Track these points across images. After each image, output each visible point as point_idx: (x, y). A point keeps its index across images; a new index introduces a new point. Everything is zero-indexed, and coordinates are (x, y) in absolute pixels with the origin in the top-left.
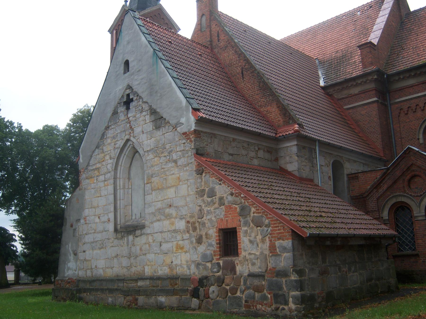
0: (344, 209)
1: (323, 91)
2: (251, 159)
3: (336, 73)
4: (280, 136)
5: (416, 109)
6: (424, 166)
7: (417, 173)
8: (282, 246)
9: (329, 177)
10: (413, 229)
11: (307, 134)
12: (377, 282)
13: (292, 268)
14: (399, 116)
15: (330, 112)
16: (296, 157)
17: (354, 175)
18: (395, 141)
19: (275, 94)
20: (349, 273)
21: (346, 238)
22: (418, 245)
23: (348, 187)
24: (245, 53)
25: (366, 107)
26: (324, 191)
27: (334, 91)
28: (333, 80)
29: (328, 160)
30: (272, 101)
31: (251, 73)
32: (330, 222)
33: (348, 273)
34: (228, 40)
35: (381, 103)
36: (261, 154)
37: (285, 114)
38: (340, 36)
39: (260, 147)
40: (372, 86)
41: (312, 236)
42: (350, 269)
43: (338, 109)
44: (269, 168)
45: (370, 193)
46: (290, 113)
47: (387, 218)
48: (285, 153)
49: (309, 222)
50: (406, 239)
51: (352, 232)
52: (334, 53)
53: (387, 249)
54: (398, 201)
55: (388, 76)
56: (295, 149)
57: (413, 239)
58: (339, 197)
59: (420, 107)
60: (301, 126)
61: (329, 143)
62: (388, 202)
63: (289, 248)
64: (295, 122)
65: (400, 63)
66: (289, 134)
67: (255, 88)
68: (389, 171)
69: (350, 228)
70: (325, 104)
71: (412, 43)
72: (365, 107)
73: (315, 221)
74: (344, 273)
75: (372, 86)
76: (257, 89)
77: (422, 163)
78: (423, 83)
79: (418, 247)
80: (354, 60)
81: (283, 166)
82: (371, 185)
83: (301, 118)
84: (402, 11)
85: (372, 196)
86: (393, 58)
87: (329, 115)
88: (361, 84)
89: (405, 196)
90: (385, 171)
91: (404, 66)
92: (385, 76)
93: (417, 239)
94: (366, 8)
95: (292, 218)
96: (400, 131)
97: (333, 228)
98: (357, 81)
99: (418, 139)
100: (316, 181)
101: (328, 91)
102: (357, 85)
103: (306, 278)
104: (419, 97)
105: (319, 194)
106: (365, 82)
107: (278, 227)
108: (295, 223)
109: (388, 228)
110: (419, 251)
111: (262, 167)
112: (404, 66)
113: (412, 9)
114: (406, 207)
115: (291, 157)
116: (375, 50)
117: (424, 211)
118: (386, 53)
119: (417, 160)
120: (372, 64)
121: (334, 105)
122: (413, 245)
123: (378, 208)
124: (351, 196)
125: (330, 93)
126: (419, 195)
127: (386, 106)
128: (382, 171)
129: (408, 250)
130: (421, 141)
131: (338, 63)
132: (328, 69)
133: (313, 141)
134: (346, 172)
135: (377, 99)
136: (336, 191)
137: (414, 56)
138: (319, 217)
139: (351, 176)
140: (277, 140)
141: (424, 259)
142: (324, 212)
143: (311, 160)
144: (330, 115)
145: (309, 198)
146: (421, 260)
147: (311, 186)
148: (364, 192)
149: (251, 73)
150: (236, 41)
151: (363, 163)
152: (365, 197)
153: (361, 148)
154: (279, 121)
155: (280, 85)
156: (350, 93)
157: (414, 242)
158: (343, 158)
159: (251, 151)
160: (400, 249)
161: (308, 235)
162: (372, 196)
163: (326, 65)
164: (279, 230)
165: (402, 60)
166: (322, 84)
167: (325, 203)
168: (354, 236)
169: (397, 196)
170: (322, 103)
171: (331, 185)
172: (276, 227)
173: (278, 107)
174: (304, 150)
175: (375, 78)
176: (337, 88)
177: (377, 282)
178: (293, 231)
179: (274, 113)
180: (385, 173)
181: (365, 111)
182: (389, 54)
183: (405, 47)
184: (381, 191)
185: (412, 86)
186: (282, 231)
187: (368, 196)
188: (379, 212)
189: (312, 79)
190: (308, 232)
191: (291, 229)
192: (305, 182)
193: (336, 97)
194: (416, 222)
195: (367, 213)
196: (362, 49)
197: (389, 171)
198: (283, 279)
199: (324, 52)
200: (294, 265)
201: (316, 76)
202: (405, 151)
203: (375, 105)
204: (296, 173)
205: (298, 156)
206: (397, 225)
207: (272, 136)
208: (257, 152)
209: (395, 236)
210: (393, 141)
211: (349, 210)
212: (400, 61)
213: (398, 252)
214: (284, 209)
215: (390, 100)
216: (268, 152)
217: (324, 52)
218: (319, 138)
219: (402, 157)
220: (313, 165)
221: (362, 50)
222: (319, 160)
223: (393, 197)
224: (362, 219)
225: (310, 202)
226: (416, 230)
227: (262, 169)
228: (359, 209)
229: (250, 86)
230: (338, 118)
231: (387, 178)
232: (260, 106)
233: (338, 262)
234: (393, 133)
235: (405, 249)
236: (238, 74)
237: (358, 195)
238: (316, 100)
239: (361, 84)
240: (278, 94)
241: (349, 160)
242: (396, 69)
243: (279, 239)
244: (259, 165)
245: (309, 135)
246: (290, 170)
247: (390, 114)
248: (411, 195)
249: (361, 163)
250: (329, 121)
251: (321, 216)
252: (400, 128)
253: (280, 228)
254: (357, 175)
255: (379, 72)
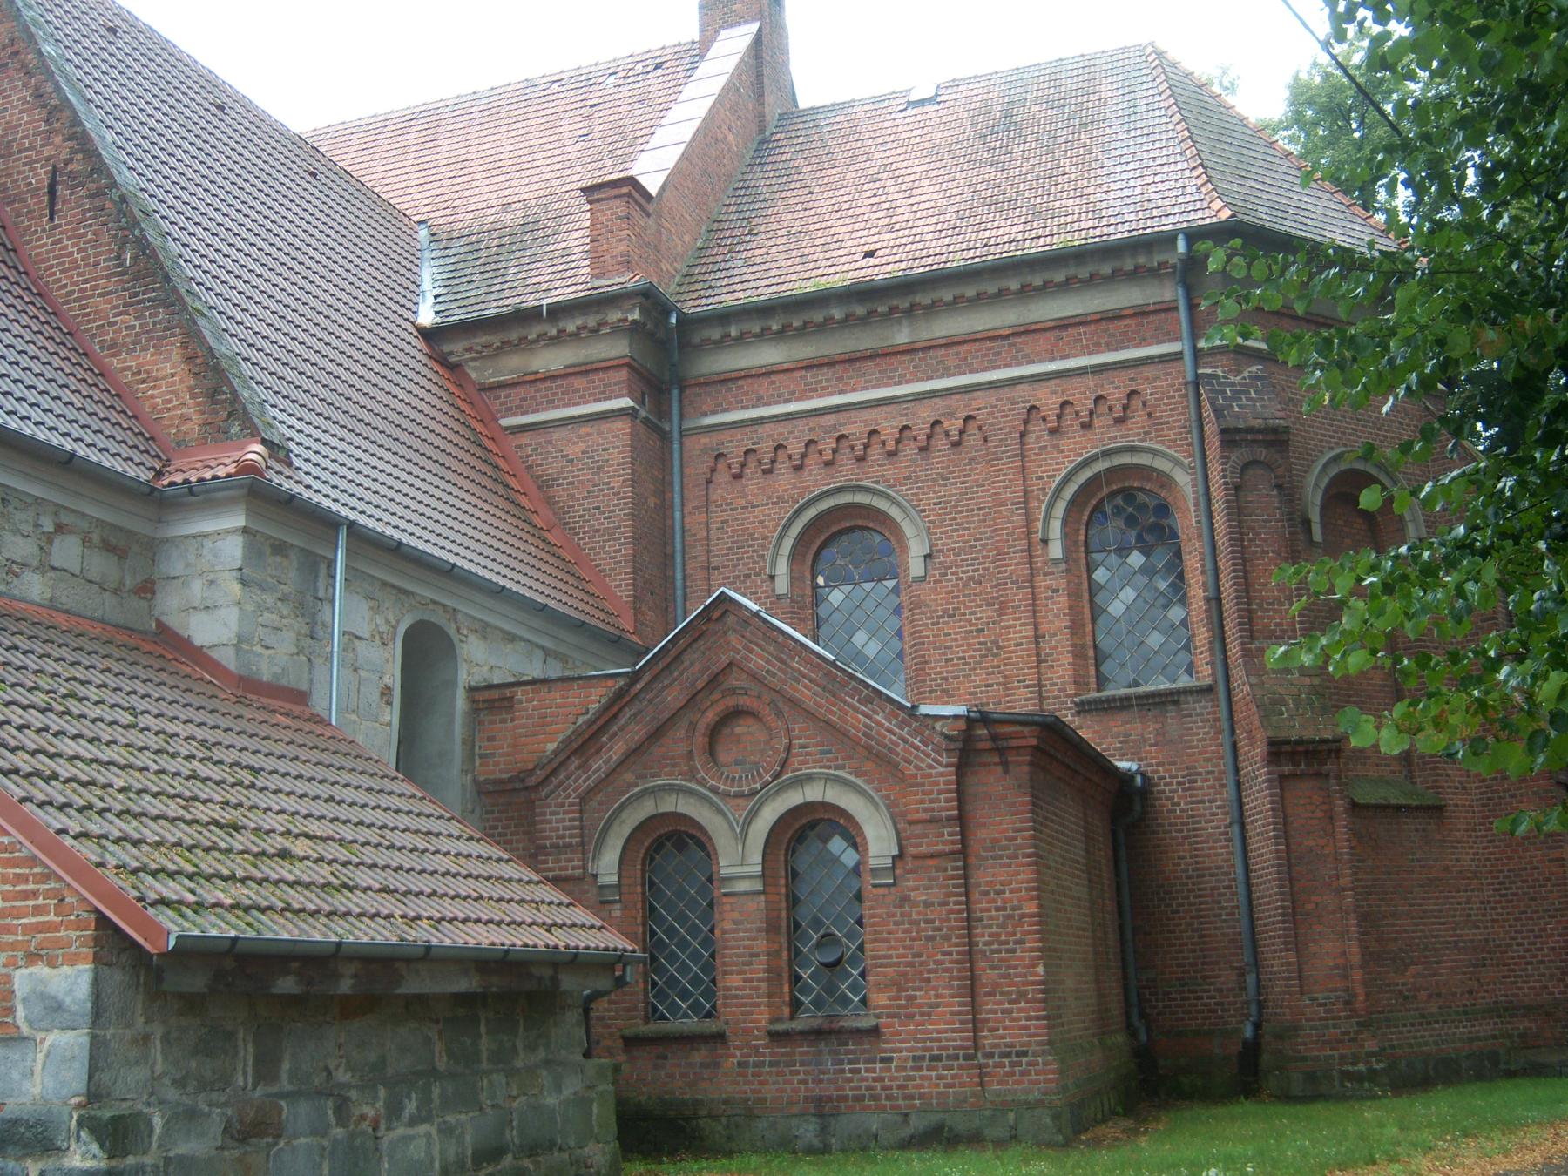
0: (416, 832)
1: (421, 344)
2: (9, 571)
3: (489, 282)
4: (172, 484)
5: (773, 461)
6: (774, 675)
7: (744, 701)
8: (43, 997)
9: (386, 692)
10: (712, 931)
11: (297, 489)
12: (527, 1163)
13: (79, 1106)
14: (709, 482)
15: (438, 429)
16: (236, 588)
17: (496, 694)
18: (684, 578)
19: (180, 299)
20: (388, 1129)
21: (382, 964)
22: (726, 998)
23: (469, 743)
24: (80, 108)
25: (586, 429)
26: (343, 747)
27: (470, 350)
28: (470, 309)
29: (391, 618)
30: (166, 329)
31: (92, 196)
32: (323, 887)
33: (383, 1126)
34: (12, 40)
35: (646, 421)
36: (67, 552)
37: (212, 394)
38: (526, 151)
39: (65, 519)
40: (619, 348)
41: (191, 952)
42: (394, 1110)
43: (474, 424)
44: (102, 621)
45: (554, 772)
46: (234, 393)
47: (614, 879)
48: (188, 565)
49: (208, 878)
50: (684, 968)
51: (422, 934)
52: (493, 211)
53: (587, 1011)
54: (661, 810)
55: (684, 320)
56: (233, 550)
57: (708, 968)
58: (421, 785)
59: (790, 457)
60: (282, 454)
61: (400, 543)
62: (624, 815)
63: (74, 1008)
64: (251, 431)
65: (737, 279)
66: (215, 477)
67: (97, 264)
68: (638, 686)
69: (418, 917)
70: (422, 393)
71: (790, 216)
72: (584, 430)
73: (240, 873)
74: (365, 1125)
75: (619, 348)
76: (108, 268)
77: (768, 662)
78: (809, 367)
79: (725, 1005)
80: (564, 245)
81: (173, 621)
82: (560, 737)
83: (285, 423)
84: (769, 99)
85: (561, 783)
86: (711, 259)
87: (431, 438)
88: (575, 336)
89: (691, 792)
90: (621, 682)
91: (748, 293)
92: (674, 320)
93: (725, 973)
94: (640, 66)
95: (117, 855)
96: (708, 538)
97: (329, 915)
98: (561, 325)
99: (772, 577)
100: (318, 704)
101: (446, 348)
102: (560, 339)
103: (148, 1160)
104: (789, 417)
105: (316, 756)
106: (595, 331)
107: (34, 894)
108: (122, 882)
109: (598, 923)
110: (727, 1023)
111: (67, 612)
112: (748, 293)
113: (804, 103)
114: (692, 837)
115: (212, 582)
116: (648, 215)
117: (756, 857)
118: (687, 238)
119: (751, 651)
120: (627, 264)
121: (463, 406)
122: (710, 994)
123: (582, 836)
124: (475, 781)
125: (453, 359)
126: (746, 790)
127: (665, 437)
128: (610, 683)
129: (686, 1015)
130: (782, 586)
131: (503, 250)
132: (461, 265)
133: (326, 523)
134: (465, 676)
135: (632, 404)
136: (412, 757)
137: (789, 262)
138: (271, 857)
139: (486, 695)
140: (161, 501)
141: (743, 1055)
142: (307, 836)
143: (308, 608)
144: (437, 441)
145: (256, 771)
146: (734, 1056)
147: (285, 721)
148: (530, 766)
149: (92, 196)
150: (48, 49)
151: (543, 648)
152: (536, 788)
153: (542, 588)
154: (185, 419)
155: (299, 349)
156: (534, 369)
157: (714, 981)
158: (460, 616)
159: (16, 532)
160: (655, 1009)
161: (172, 944)
162: (561, 783)
163: (454, 251)
164: (38, 910)
165: (744, 270)
166: (426, 317)
167: (331, 799)
168: (428, 956)
169: (662, 788)
170: (410, 386)
171: (389, 724)
172: (26, 895)
173: (189, 359)
174: (278, 559)
175: (634, 321)
176: (480, 340)
177: (527, 1163)
178: (102, 921)
179: (166, 380)
180: (620, 694)
181: (582, 446)
182: (699, 243)
183: (762, 228)
184: (599, 766)
185: (768, 373)
186: (52, 917)
187: (545, 781)
188: (584, 853)
189: (385, 290)
190: (173, 928)
191: (97, 911)
192: (265, 701)
193: (473, 375)
194: (725, 900)
195: (533, 856)
196: (598, 201)
197: (638, 686)
198: (29, 1163)
199: (456, 203)
200: (94, 1095)
201: (407, 283)
202: (706, 607)
203: (623, 426)
204: (227, 658)
205: (243, 582)
206: (652, 909)
207: (135, 480)
208: (50, 542)
209: (621, 959)
210: (679, 576)
211: (438, 835)
212: (736, 272)
213: (647, 1020)
214: (90, 807)
215: (682, 417)
216: (108, 547)
217: (456, 203)
218: (353, 516)
219: (695, 633)
220: (315, 631)
221: (596, 205)
222: (345, 610)
223: (644, 793)
224: (488, 878)
225: (253, 786)
226: (724, 932)
227: (60, 619)
228: (491, 834)
229: (80, 251)
230: (467, 458)
231: (629, 712)
232: (111, 347)
233: (343, 1076)
234: (678, 547)
235: (674, 1009)
236: (34, 192)
237: (505, 776)
238: (386, 372)
239: (575, 336)
240: (197, 305)
241: (483, 630)
242: (717, 299)
243: (32, 958)
244: (52, 605)
245: (306, 494)
246: (200, 639)
247: (676, 469)
248: (714, 790)
249: (537, 646)
250: (422, 461)
251: (284, 854)
252: (708, 530)
253: (40, 901)
254: (508, 692)
255: (648, 297)
